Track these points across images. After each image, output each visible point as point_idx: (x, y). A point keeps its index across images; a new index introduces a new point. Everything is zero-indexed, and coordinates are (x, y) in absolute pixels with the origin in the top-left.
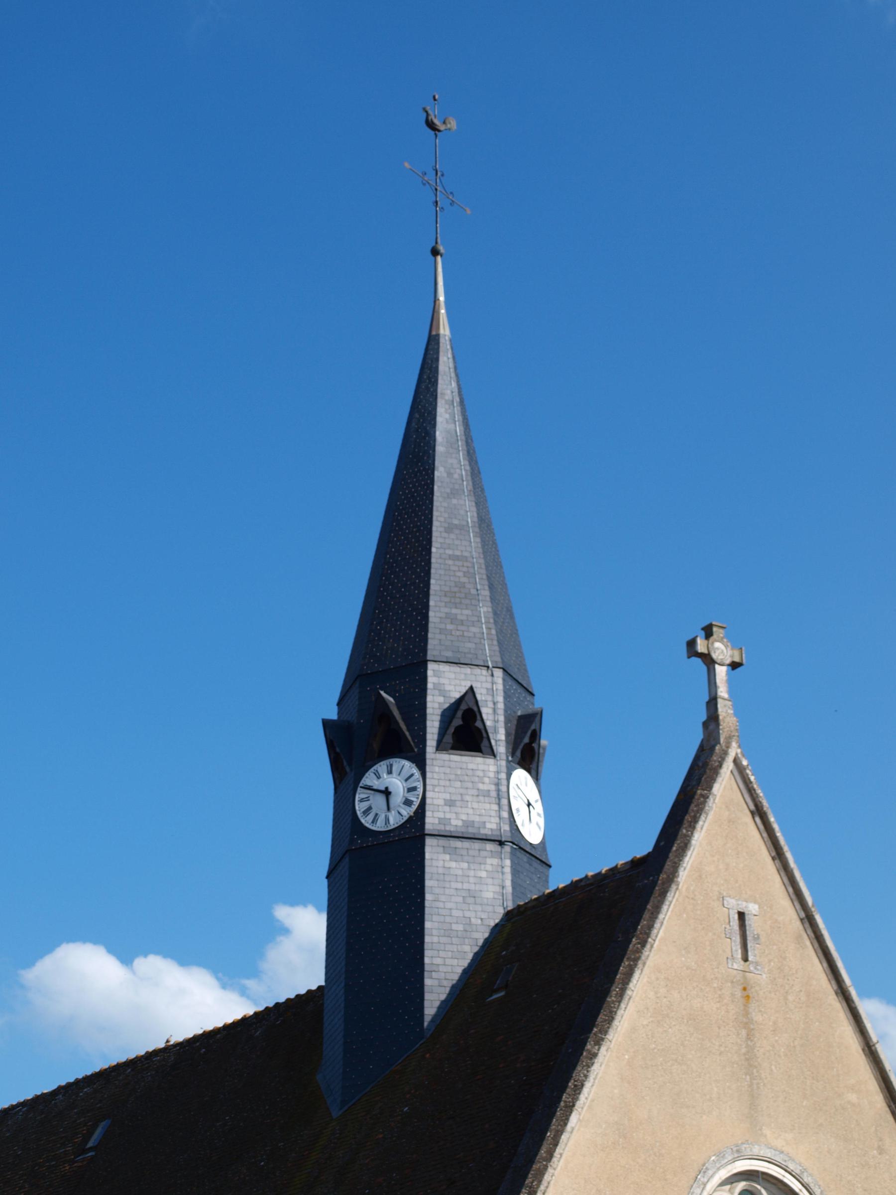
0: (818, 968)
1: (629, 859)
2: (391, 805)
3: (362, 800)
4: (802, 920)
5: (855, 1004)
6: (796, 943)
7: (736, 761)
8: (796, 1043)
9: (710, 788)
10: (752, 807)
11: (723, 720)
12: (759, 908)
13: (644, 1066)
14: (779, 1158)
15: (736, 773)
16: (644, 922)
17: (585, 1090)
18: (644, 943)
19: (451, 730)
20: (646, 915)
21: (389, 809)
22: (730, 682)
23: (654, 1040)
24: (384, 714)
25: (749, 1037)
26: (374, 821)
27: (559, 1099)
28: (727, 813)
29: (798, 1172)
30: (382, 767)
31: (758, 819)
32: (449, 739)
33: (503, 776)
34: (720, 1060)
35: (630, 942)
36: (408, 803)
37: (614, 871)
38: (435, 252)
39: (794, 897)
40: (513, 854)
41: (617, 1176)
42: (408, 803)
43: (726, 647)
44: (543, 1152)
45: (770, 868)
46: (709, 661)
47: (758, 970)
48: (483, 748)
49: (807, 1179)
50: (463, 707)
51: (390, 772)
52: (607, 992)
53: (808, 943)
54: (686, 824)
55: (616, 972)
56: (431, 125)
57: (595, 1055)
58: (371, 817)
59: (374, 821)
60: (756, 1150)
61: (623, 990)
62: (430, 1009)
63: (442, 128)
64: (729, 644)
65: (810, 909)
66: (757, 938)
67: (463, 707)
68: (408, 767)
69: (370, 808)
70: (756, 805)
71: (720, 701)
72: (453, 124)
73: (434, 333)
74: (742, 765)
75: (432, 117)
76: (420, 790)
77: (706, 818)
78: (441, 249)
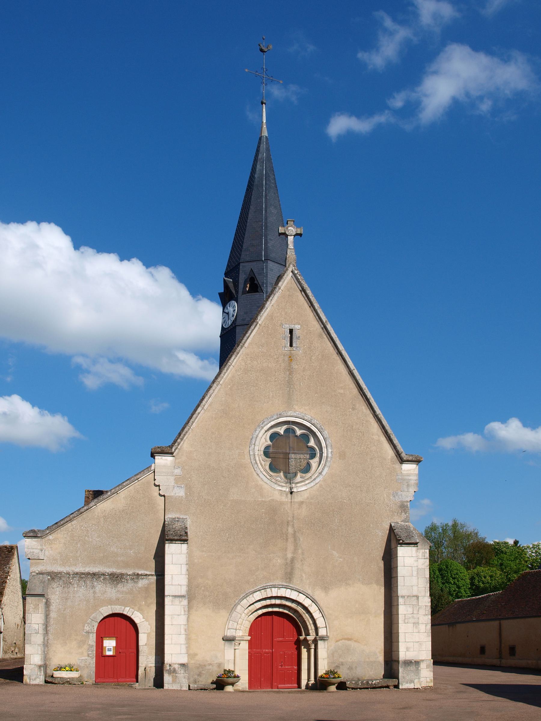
2: (229, 318)
4: (322, 328)
5: (344, 357)
6: (319, 337)
8: (314, 374)
10: (301, 289)
11: (289, 257)
12: (301, 327)
13: (237, 389)
15: (293, 276)
23: (243, 379)
25: (290, 374)
28: (288, 293)
29: (309, 420)
31: (303, 293)
34: (275, 384)
36: (233, 316)
38: (262, 103)
39: (319, 320)
41: (221, 427)
43: (294, 228)
47: (297, 349)
48: (259, 291)
53: (325, 337)
56: (262, 50)
60: (289, 413)
64: (295, 227)
65: (324, 323)
70: (302, 288)
72: (271, 47)
74: (295, 273)
77: (274, 296)
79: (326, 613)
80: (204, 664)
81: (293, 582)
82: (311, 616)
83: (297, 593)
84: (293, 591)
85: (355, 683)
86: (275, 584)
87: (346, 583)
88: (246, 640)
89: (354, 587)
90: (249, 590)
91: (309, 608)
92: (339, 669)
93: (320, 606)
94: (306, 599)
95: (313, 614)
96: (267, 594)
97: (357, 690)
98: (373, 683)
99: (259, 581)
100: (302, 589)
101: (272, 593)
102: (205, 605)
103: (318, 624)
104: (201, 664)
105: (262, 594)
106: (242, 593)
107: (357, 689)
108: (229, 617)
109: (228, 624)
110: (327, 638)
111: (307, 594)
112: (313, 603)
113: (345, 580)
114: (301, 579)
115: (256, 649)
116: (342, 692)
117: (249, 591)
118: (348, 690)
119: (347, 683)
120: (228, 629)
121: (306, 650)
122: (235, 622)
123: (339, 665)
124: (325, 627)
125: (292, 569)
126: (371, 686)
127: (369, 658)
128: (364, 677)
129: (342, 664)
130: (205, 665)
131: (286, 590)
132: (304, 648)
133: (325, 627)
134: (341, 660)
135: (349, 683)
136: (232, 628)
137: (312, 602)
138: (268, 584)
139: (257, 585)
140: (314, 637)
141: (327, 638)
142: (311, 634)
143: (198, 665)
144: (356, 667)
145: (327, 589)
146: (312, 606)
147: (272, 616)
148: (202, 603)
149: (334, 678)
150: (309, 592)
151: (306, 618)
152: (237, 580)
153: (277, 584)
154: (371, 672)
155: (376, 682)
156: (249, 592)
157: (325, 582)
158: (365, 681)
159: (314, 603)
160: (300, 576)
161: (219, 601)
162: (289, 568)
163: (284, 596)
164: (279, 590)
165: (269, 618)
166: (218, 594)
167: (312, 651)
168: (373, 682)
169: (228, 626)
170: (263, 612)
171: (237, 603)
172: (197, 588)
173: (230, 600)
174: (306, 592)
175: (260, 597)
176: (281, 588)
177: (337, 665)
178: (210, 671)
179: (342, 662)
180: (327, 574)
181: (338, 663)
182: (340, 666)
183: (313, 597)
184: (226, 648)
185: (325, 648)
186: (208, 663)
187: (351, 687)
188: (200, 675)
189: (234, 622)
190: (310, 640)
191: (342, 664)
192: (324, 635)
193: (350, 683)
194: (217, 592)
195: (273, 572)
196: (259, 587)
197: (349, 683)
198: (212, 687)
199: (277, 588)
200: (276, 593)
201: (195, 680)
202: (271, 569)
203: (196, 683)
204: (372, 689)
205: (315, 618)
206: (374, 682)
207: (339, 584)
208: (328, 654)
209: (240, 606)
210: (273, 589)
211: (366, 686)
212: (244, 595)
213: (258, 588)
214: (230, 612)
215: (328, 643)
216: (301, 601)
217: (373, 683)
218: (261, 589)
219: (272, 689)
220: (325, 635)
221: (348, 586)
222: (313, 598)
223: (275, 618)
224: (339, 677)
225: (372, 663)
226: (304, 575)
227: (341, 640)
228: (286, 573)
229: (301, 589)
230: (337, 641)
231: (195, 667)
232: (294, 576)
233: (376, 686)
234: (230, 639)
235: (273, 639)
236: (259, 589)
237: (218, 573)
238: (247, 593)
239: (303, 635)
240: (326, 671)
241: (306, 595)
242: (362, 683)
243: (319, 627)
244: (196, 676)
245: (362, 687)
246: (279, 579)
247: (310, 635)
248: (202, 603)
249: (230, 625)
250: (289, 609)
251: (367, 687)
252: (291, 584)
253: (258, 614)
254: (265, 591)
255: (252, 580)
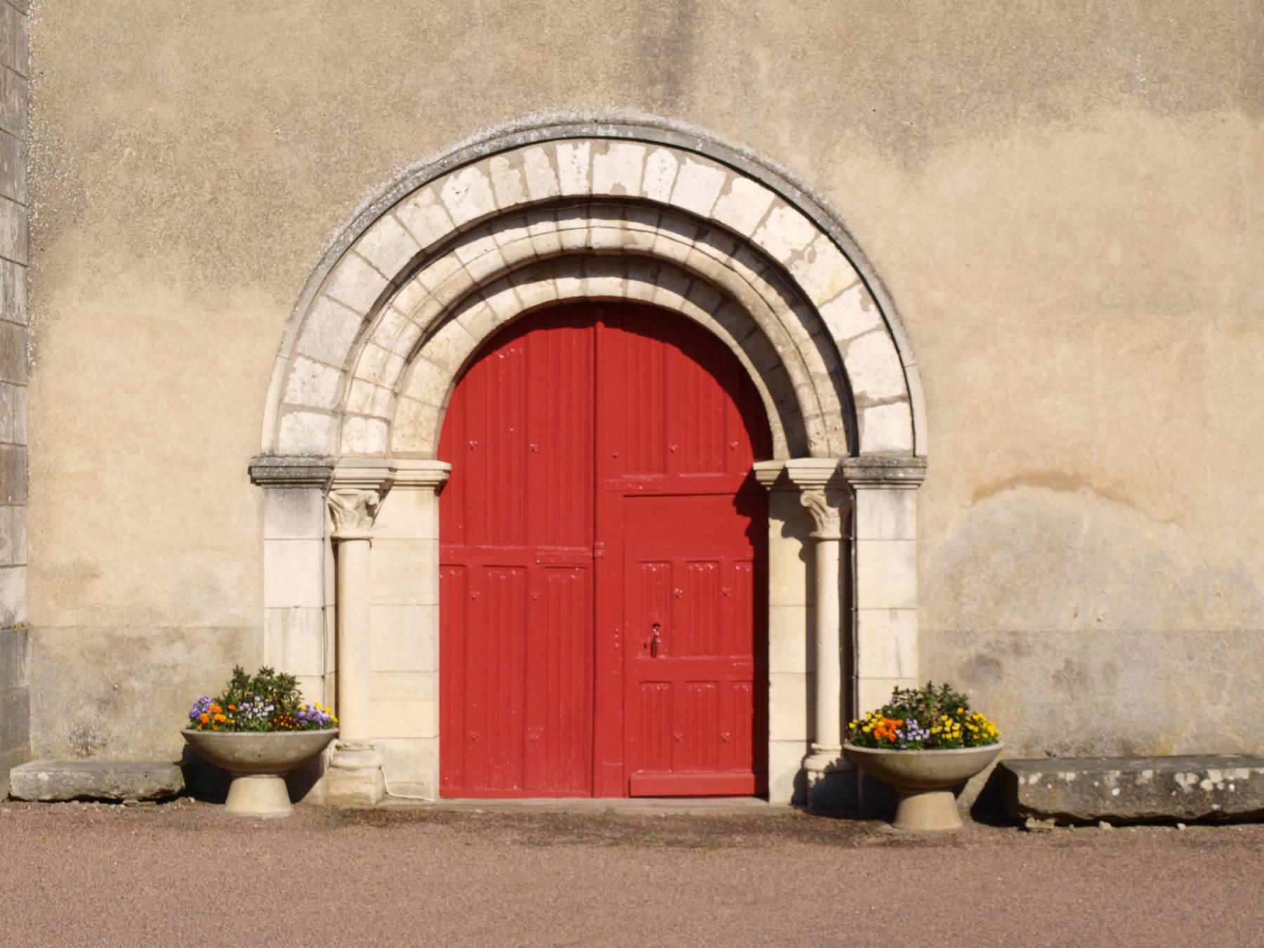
79: (907, 306)
80: (134, 634)
81: (692, 102)
82: (817, 329)
83: (717, 175)
84: (690, 163)
85: (1077, 785)
86: (573, 117)
87: (1041, 106)
88: (418, 485)
89: (1095, 129)
90: (410, 161)
91: (799, 274)
92: (999, 677)
93: (865, 259)
94: (776, 211)
95: (824, 312)
96: (523, 180)
97: (1092, 829)
98: (1206, 785)
99: (473, 96)
100: (748, 150)
101: (557, 177)
102: (140, 256)
103: (858, 375)
104: (118, 633)
105: (491, 185)
106: (370, 180)
107: (1094, 822)
108: (284, 333)
109: (285, 380)
110: (912, 473)
111: (784, 177)
112: (824, 238)
113: (1033, 86)
114: (746, 84)
115: (495, 542)
116: (991, 835)
117: (413, 166)
118: (1028, 830)
119: (1022, 781)
120: (284, 408)
121: (795, 545)
122: (326, 365)
123: (995, 655)
124: (902, 399)
125: (683, 17)
126: (1192, 808)
127: (1197, 612)
128: (1162, 738)
129: (1017, 650)
130: (143, 643)
131: (648, 154)
132: (786, 533)
133: (902, 399)
134: (1010, 619)
135: (1034, 779)
136: (313, 404)
137: (812, 230)
138: (533, 119)
139: (459, 128)
140: (833, 463)
141: (912, 473)
142: (817, 445)
143: (103, 642)
144: (1110, 671)
145: (913, 143)
146: (819, 258)
147: (592, 329)
148: (128, 247)
149: (931, 743)
150: (798, 165)
151: (783, 338)
152: (335, 97)
153: (588, 116)
154: (1215, 704)
155: (1226, 782)
156: (415, 172)
157: (901, 99)
158: (1148, 774)
159: (832, 240)
160: (734, 63)
161: (228, 232)
162: (668, 11)
163: (632, 191)
164: (604, 157)
165: (571, 338)
166: (222, 184)
167: (830, 555)
168: (1203, 776)
169: (283, 392)
170: (521, 302)
171: (338, 242)
172: (93, 149)
173: (292, 225)
174: (778, 166)
175: (478, 205)
176: (614, 145)
177: (984, 651)
178: (177, 679)
179: (1014, 633)
180: (914, 42)
181: (991, 637)
182: (1003, 660)
183: (825, 202)
184: (270, 532)
185: (899, 537)
186: (164, 624)
187: (1051, 809)
188: (111, 701)
189: (319, 368)
190: (811, 486)
191: (1017, 650)
192: (892, 452)
193: (1043, 782)
194: (214, 177)
195: (560, 41)
196: (478, 138)
197: (1034, 779)
198: (146, 786)
199: (588, 143)
200: (584, 173)
201: (85, 734)
202: (548, 21)
203: (89, 754)
204: (1197, 829)
205: (838, 336)
206: (1215, 777)
207: (996, 108)
208: (919, 574)
209: (359, 260)
210: (564, 150)
211: (1153, 807)
212: (382, 190)
213: (469, 142)
214: (296, 305)
215: (919, 505)
216: (744, 229)
217: (1206, 785)
218: (486, 149)
219: (592, 796)
220: (904, 452)
221: (1054, 122)
222: (819, 205)
223: (611, 338)
224: (968, 739)
225: (1217, 646)
226: (760, 55)
227: (1012, 483)
228: (646, 45)
229: (745, 147)
230: (981, 493)
231: (82, 653)
232: (696, 59)
233: (1229, 810)
234: (293, 473)
235: (599, 479)
236: (476, 149)
237: (221, 56)
238: (399, 177)
239: (776, 454)
240: (896, 693)
241: (774, 185)
242: (1128, 780)
243: (863, 396)
244: (88, 712)
245: (1129, 811)
246: (602, 85)
247: (813, 449)
248: (128, 247)
249: (299, 385)
250: (686, 283)
251: (1161, 811)
252: (676, 114)
253: (494, 318)
254: (511, 167)
255: (429, 94)
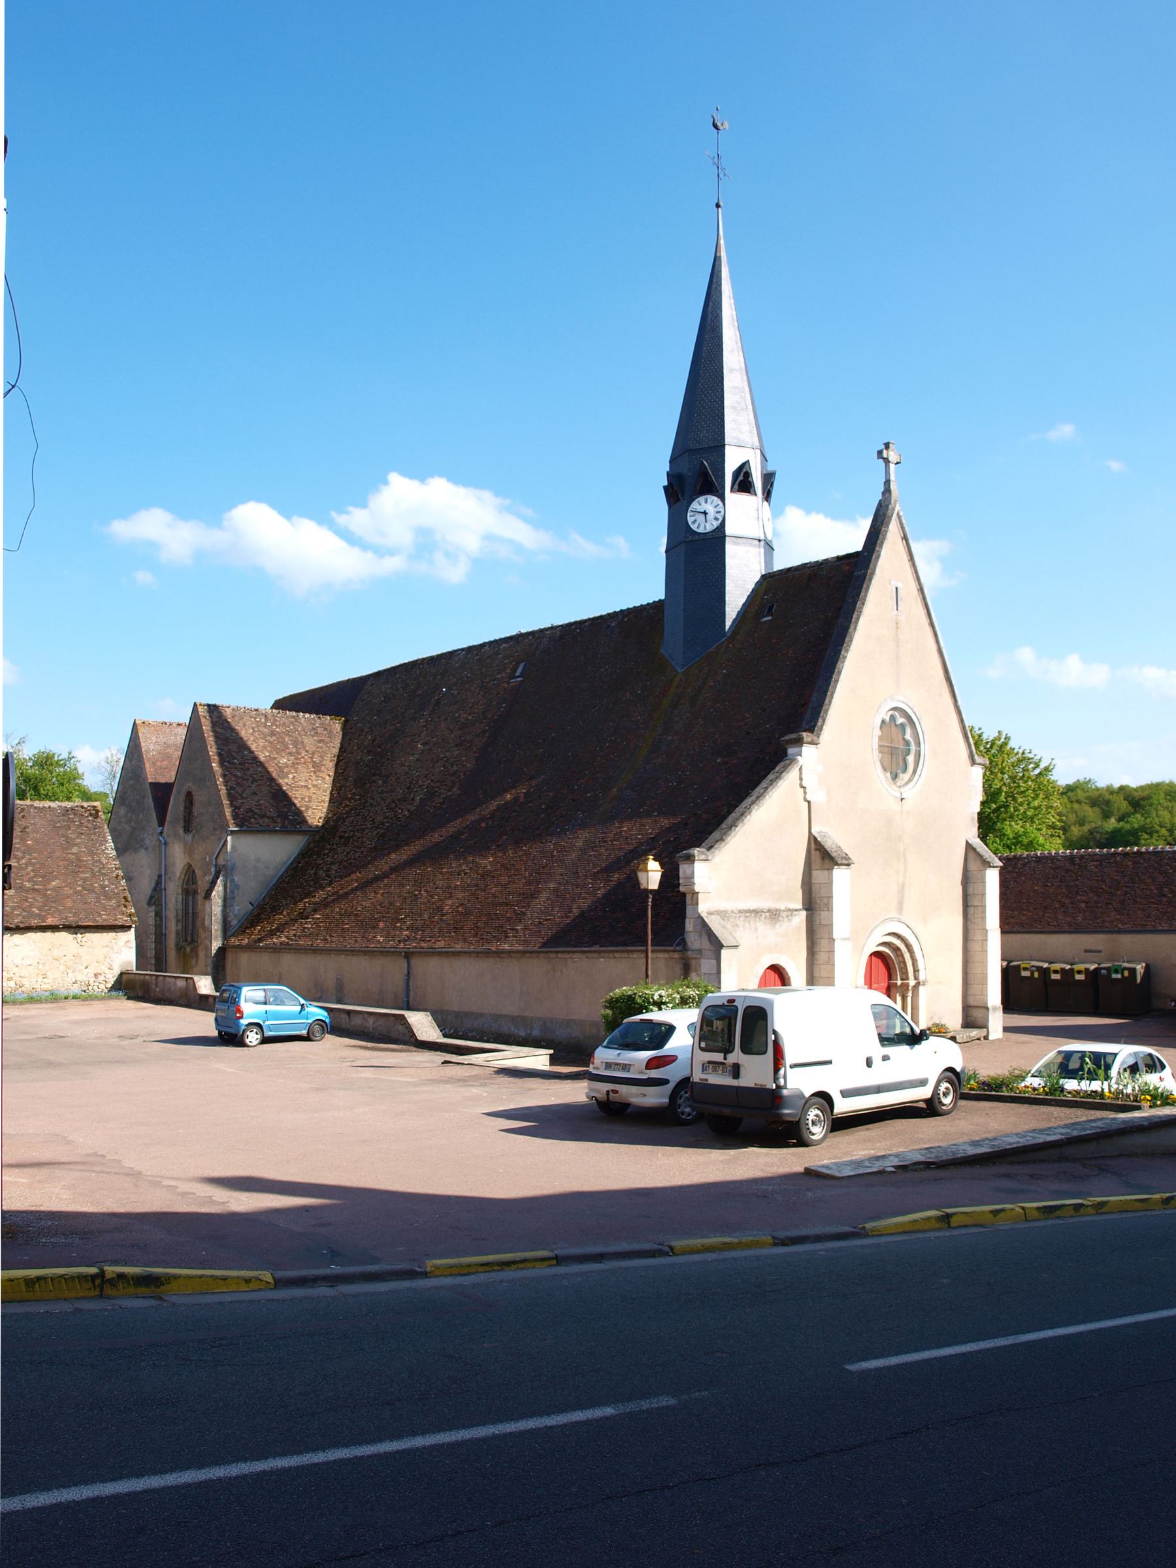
0: (923, 612)
1: (836, 555)
3: (691, 516)
7: (898, 514)
9: (888, 527)
10: (902, 535)
14: (906, 701)
16: (862, 594)
17: (843, 673)
18: (863, 604)
19: (737, 483)
20: (863, 590)
21: (706, 521)
22: (896, 470)
24: (706, 474)
26: (698, 527)
27: (831, 677)
30: (702, 499)
31: (904, 541)
32: (736, 486)
33: (760, 506)
35: (856, 603)
36: (716, 519)
37: (827, 560)
40: (764, 547)
42: (716, 519)
44: (827, 701)
45: (908, 565)
46: (887, 461)
49: (915, 710)
50: (744, 470)
51: (706, 502)
52: (848, 627)
54: (878, 545)
55: (852, 618)
56: (715, 126)
57: (846, 657)
58: (696, 525)
59: (698, 527)
61: (856, 627)
62: (728, 624)
63: (721, 128)
66: (902, 599)
67: (744, 470)
68: (716, 500)
69: (695, 520)
71: (891, 483)
72: (726, 125)
73: (718, 255)
75: (716, 121)
76: (723, 513)
78: (721, 204)
